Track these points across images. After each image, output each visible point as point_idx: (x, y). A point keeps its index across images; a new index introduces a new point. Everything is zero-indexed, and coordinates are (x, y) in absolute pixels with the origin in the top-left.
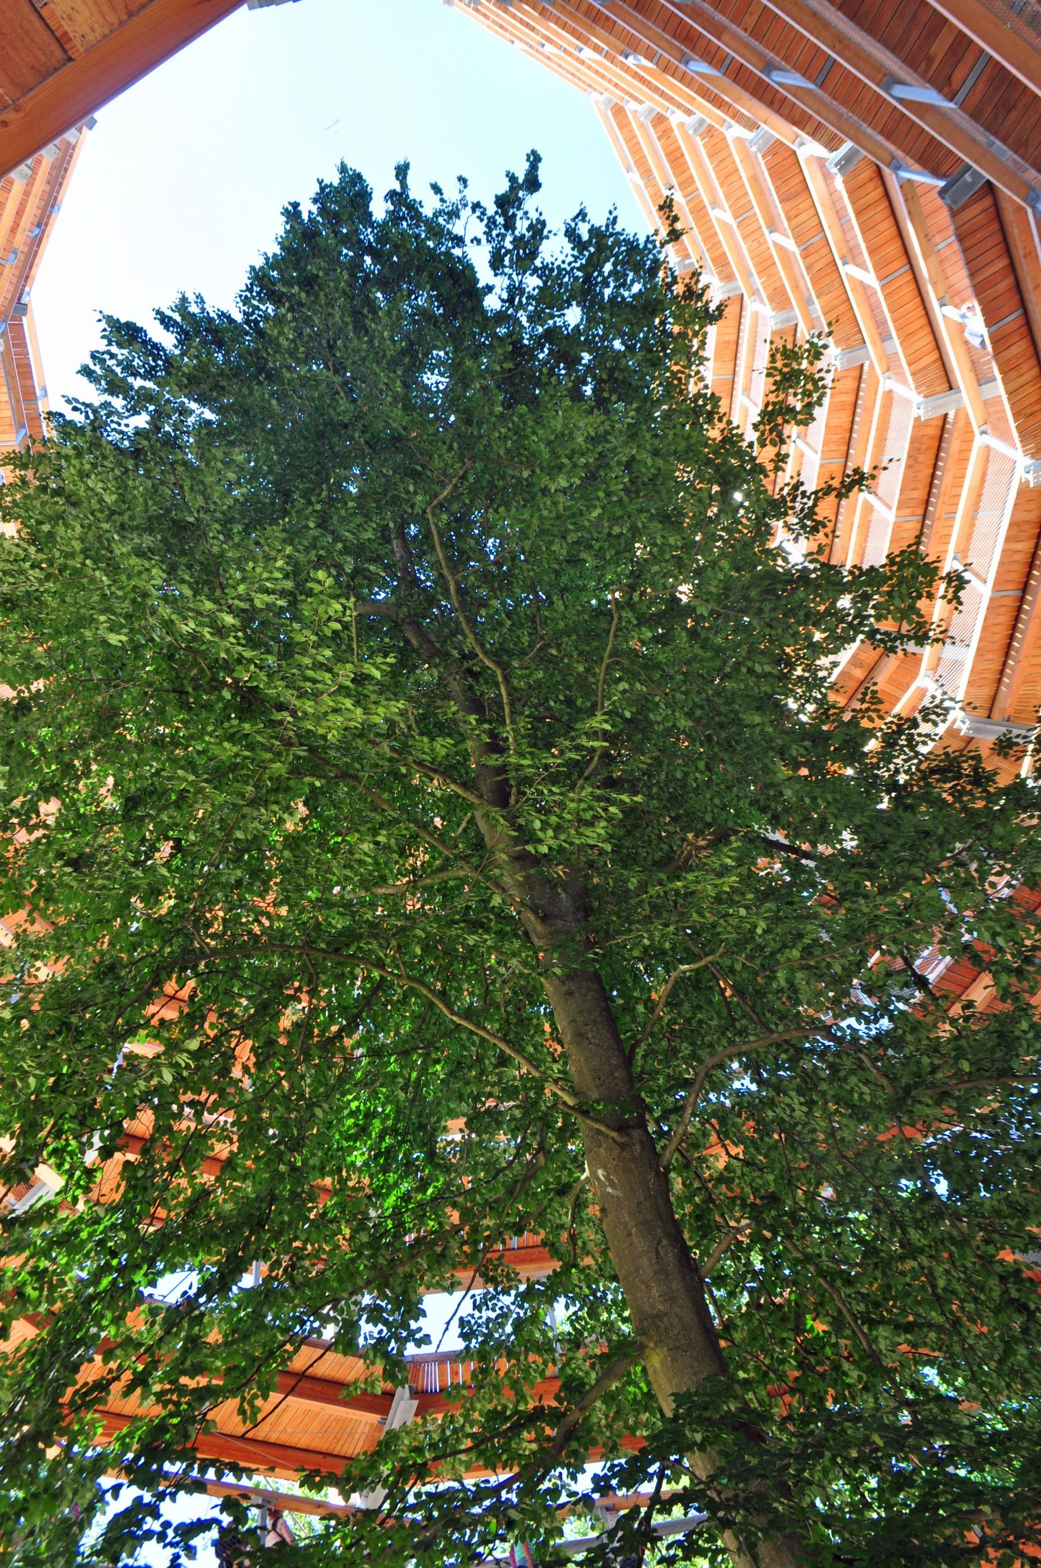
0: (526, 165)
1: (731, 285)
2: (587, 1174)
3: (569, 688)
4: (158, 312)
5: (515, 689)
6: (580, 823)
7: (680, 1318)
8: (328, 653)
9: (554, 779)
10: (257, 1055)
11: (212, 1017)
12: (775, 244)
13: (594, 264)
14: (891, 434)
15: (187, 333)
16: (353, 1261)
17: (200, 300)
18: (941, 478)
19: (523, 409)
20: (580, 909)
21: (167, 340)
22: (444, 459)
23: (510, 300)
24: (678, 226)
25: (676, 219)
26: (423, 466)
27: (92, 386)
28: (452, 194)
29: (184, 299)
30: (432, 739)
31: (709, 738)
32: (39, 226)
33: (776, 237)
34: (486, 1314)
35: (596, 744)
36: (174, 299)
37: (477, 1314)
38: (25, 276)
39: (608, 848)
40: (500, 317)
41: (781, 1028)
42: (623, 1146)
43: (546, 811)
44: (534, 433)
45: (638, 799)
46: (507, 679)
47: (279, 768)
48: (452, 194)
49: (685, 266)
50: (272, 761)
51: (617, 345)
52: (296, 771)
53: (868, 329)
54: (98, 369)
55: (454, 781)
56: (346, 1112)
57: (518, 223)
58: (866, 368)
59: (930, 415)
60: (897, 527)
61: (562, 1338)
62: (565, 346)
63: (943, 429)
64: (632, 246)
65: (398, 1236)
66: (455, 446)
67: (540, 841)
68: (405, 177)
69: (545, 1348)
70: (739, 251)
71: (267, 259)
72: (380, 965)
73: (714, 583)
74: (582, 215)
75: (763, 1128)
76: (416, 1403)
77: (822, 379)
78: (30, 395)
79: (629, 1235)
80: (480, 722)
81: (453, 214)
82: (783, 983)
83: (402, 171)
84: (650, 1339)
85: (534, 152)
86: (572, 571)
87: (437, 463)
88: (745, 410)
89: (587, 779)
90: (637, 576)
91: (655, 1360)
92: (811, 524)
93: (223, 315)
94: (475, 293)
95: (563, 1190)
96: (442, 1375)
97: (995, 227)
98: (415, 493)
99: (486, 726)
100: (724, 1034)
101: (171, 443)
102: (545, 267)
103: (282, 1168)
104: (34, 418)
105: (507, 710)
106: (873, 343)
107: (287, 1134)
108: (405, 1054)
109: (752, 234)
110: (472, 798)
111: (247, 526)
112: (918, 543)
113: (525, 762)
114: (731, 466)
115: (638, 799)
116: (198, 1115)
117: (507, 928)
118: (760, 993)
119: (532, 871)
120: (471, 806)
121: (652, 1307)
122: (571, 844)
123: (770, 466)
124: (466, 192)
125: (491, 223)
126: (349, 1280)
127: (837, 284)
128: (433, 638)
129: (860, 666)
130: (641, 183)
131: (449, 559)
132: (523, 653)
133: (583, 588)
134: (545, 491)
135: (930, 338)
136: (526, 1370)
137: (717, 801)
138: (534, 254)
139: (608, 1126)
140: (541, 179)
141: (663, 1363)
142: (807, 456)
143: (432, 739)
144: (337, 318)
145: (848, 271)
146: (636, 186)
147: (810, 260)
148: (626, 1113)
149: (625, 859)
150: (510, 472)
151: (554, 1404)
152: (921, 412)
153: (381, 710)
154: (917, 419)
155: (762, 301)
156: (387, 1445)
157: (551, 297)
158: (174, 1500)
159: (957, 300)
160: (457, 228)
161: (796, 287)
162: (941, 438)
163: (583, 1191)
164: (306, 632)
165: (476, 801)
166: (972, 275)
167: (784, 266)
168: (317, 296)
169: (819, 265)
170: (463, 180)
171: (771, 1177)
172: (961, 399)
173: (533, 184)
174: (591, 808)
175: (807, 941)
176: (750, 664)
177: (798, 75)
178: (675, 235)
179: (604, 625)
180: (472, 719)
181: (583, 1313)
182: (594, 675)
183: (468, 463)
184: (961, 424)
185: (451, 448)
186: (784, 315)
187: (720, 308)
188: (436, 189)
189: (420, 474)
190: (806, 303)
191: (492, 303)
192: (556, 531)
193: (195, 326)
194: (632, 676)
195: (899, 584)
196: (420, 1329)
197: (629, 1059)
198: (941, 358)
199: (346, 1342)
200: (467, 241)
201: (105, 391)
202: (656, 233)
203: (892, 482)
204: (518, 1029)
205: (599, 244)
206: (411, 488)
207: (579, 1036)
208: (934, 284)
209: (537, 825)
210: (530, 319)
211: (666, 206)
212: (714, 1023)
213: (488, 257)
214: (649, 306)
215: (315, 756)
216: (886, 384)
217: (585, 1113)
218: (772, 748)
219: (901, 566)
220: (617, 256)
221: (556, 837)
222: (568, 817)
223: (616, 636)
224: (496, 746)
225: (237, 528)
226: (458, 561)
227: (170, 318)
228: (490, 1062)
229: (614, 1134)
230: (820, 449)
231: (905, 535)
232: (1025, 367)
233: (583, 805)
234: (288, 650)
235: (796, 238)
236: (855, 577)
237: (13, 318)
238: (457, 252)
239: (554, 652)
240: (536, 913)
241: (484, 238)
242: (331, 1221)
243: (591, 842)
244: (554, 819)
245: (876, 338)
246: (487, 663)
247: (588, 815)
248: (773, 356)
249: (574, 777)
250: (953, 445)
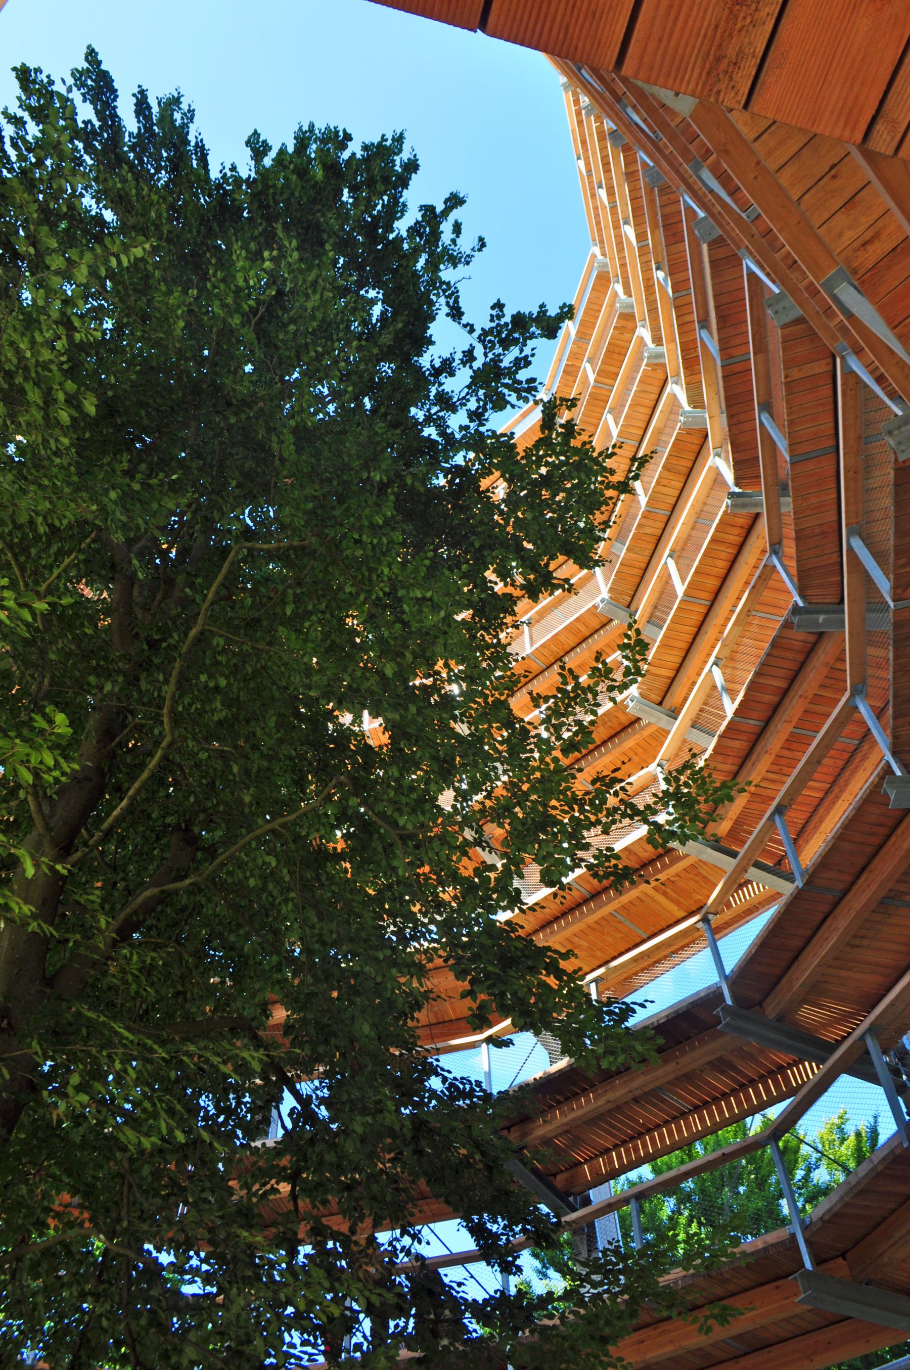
17: (190, 115)
18: (601, 755)
21: (131, 124)
83: (455, 201)
97: (801, 658)
124: (476, 254)
135: (679, 660)
144: (310, 305)
147: (646, 521)
162: (625, 728)
166: (757, 674)
168: (310, 269)
169: (648, 530)
170: (482, 243)
177: (786, 443)
193: (167, 130)
227: (149, 108)
230: (536, 646)
232: (731, 760)
241: (478, 332)
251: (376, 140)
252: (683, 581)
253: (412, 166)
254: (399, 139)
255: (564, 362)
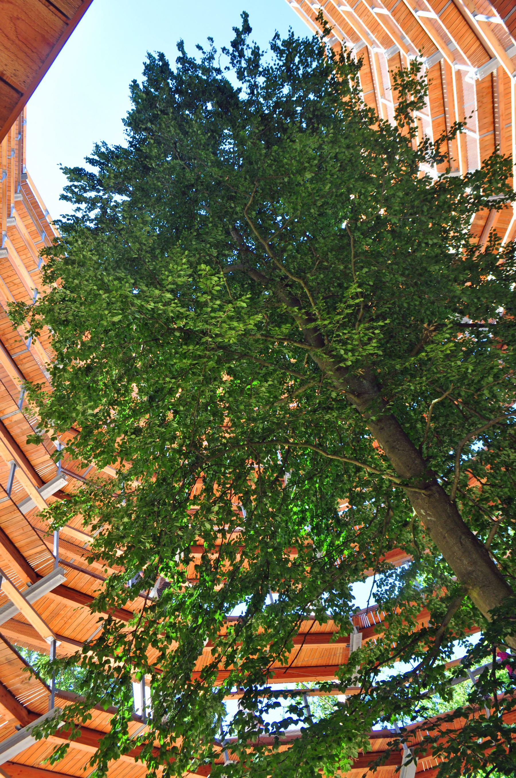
0: (242, 20)
1: (360, 43)
2: (415, 513)
3: (338, 279)
4: (87, 159)
5: (312, 287)
6: (362, 344)
7: (482, 571)
8: (218, 302)
9: (344, 326)
10: (242, 501)
11: (216, 486)
12: (377, 14)
13: (290, 60)
14: (465, 93)
15: (103, 164)
16: (314, 581)
19: (275, 148)
20: (375, 386)
21: (95, 170)
22: (244, 185)
23: (252, 92)
24: (328, 26)
25: (326, 23)
26: (236, 193)
27: (69, 202)
28: (207, 48)
29: (97, 146)
30: (280, 327)
31: (416, 283)
32: (19, 133)
33: (377, 10)
34: (384, 588)
35: (357, 301)
36: (93, 148)
37: (380, 590)
38: (21, 160)
39: (381, 353)
40: (250, 103)
41: (492, 417)
42: (429, 496)
43: (345, 343)
44: (284, 157)
45: (388, 321)
46: (306, 283)
47: (212, 364)
48: (207, 48)
49: (333, 42)
50: (207, 362)
51: (311, 96)
52: (219, 362)
53: (438, 42)
54: (70, 195)
55: (295, 342)
56: (292, 513)
57: (246, 53)
58: (442, 62)
59: (484, 76)
60: (482, 141)
61: (423, 591)
62: (286, 107)
63: (492, 81)
64: (307, 44)
65: (332, 564)
66: (248, 177)
67: (346, 360)
68: (183, 48)
69: (416, 597)
70: (358, 25)
71: (129, 113)
72: (287, 441)
73: (396, 205)
74: (277, 36)
75: (496, 468)
76: (361, 634)
77: (424, 81)
78: (41, 216)
79: (445, 538)
80: (300, 309)
81: (211, 58)
82: (488, 396)
83: (180, 46)
84: (469, 584)
85: (244, 13)
86: (323, 219)
87: (242, 189)
88: (387, 108)
89: (360, 321)
90: (355, 212)
91: (475, 594)
92: (439, 158)
93: (117, 148)
94: (234, 94)
95: (406, 524)
96: (370, 618)
98: (235, 207)
99: (303, 311)
100: (463, 427)
101: (114, 219)
102: (265, 70)
103: (270, 550)
104: (47, 226)
105: (311, 299)
106: (443, 48)
107: (267, 532)
108: (310, 479)
109: (363, 12)
110: (306, 347)
111: (162, 249)
112: (496, 150)
113: (326, 322)
114: (392, 144)
115: (388, 321)
116: (224, 536)
117: (342, 404)
118: (477, 403)
119: (347, 376)
120: (307, 351)
121: (466, 569)
122: (362, 356)
123: (408, 136)
124: (214, 44)
125: (233, 57)
126: (314, 591)
127: (415, 24)
128: (263, 273)
129: (482, 218)
130: (298, 6)
131: (261, 233)
132: (310, 268)
133: (329, 226)
134: (299, 184)
136: (410, 611)
137: (428, 312)
138: (257, 66)
139: (419, 488)
140: (251, 26)
141: (479, 594)
142: (426, 124)
143: (280, 327)
144: (173, 132)
145: (419, 15)
146: (296, 9)
147: (397, 16)
148: (425, 477)
149: (389, 354)
150: (278, 181)
151: (430, 626)
152: (478, 76)
153: (252, 322)
154: (477, 81)
155: (378, 46)
156: (354, 659)
157: (273, 83)
158: (267, 713)
159: (481, 10)
160: (215, 64)
161: (394, 33)
162: (492, 87)
163: (415, 521)
164: (205, 296)
165: (309, 348)
167: (384, 24)
170: (211, 39)
171: (506, 490)
172: (498, 62)
173: (247, 29)
174: (366, 335)
175: (495, 370)
176: (426, 241)
178: (327, 32)
179: (345, 241)
180: (296, 309)
181: (430, 576)
182: (349, 269)
183: (257, 184)
184: (501, 75)
185: (246, 179)
186: (391, 50)
187: (360, 61)
188: (199, 47)
189: (235, 197)
190: (401, 39)
191: (243, 96)
192: (310, 201)
193: (105, 157)
194: (369, 264)
195: (493, 175)
196: (354, 605)
197: (420, 452)
198: (481, 44)
199: (321, 618)
200: (222, 69)
201: (75, 202)
202: (317, 33)
203: (474, 122)
204: (361, 452)
205: (289, 48)
206: (233, 205)
207: (392, 448)
208: (467, 6)
209: (342, 352)
210: (265, 99)
211: (319, 18)
212: (458, 423)
213: (236, 75)
214: (323, 72)
215: (227, 352)
216: (455, 68)
217: (407, 485)
218: (450, 280)
219: (492, 165)
220: (300, 52)
221: (353, 355)
222: (356, 343)
223: (354, 247)
224: (311, 319)
225: (158, 251)
226: (264, 231)
227: (93, 159)
228: (352, 471)
229: (423, 491)
231: (487, 143)
233: (362, 335)
234: (200, 305)
235: (386, 7)
236: (469, 179)
237: (22, 182)
238: (219, 77)
239: (326, 264)
240: (353, 394)
242: (299, 566)
243: (371, 352)
244: (349, 347)
245: (444, 45)
246: (294, 279)
247: (366, 339)
248: (395, 78)
249: (353, 321)
250: (500, 88)
251: (143, 67)
252: (428, 10)
253: (162, 56)
254: (150, 56)
255: (309, 18)
